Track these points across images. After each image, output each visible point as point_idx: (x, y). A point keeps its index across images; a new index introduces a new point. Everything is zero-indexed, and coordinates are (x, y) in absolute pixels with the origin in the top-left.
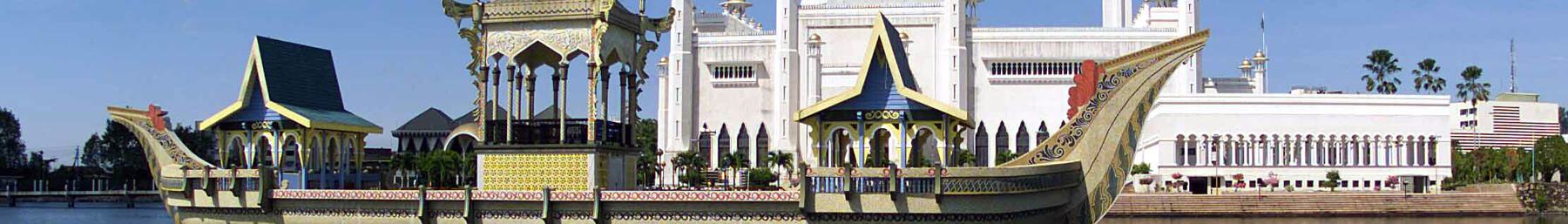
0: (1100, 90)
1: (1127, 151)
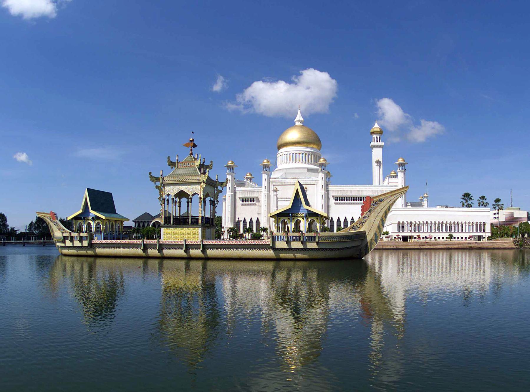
0: (372, 206)
1: (381, 227)
